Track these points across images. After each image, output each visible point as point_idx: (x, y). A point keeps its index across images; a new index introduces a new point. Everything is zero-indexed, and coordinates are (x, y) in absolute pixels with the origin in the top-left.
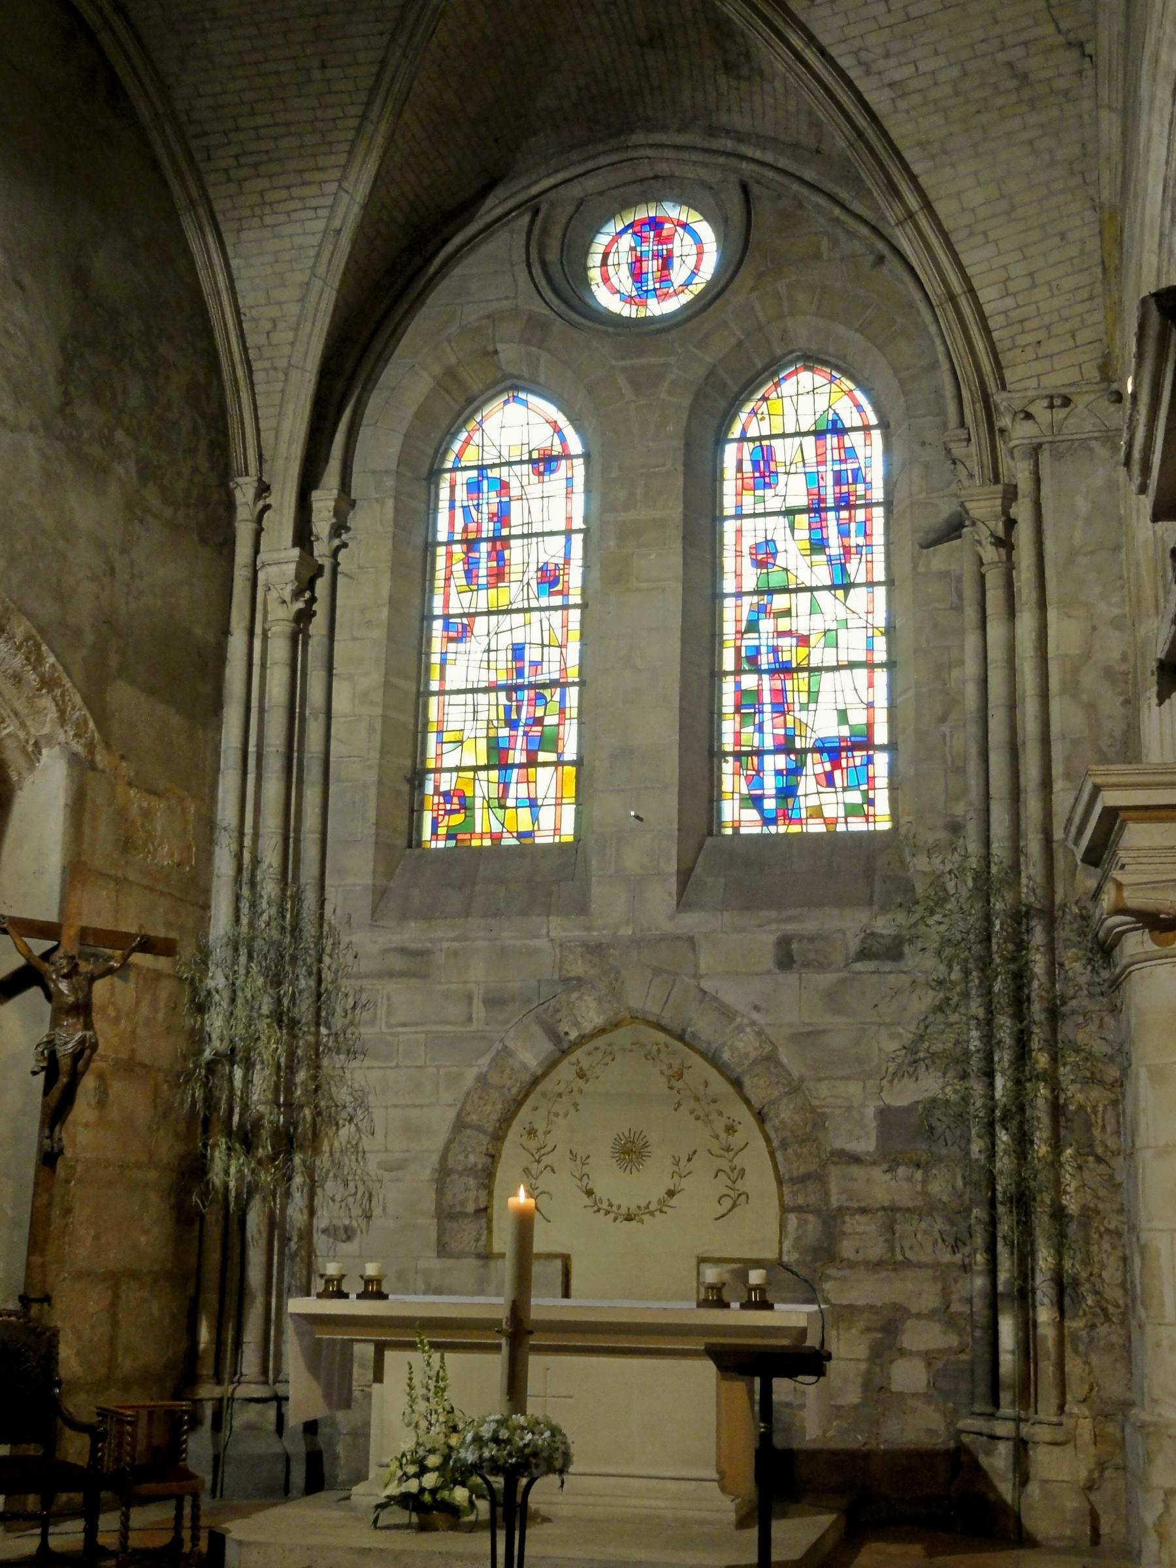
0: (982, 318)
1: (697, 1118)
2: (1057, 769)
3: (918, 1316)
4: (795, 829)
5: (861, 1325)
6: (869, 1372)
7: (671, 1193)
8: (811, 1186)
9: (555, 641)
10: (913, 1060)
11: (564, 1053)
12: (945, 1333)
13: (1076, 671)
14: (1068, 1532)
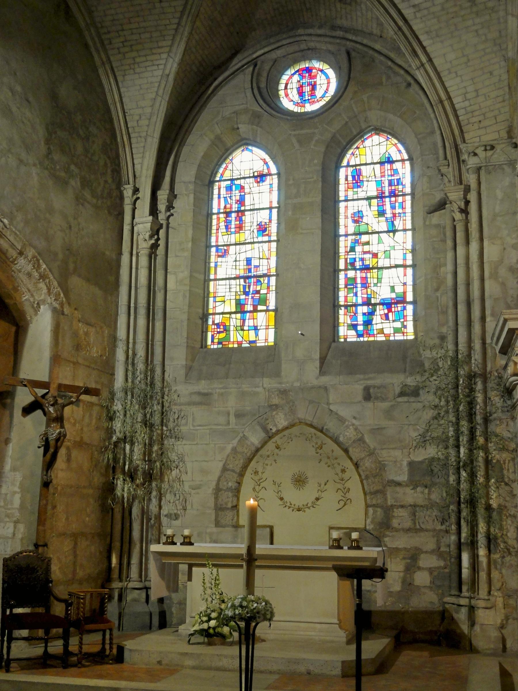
0: (455, 111)
1: (329, 466)
2: (488, 312)
3: (426, 552)
4: (371, 339)
7: (317, 499)
8: (379, 496)
9: (266, 257)
10: (424, 441)
11: (270, 438)
12: (438, 560)
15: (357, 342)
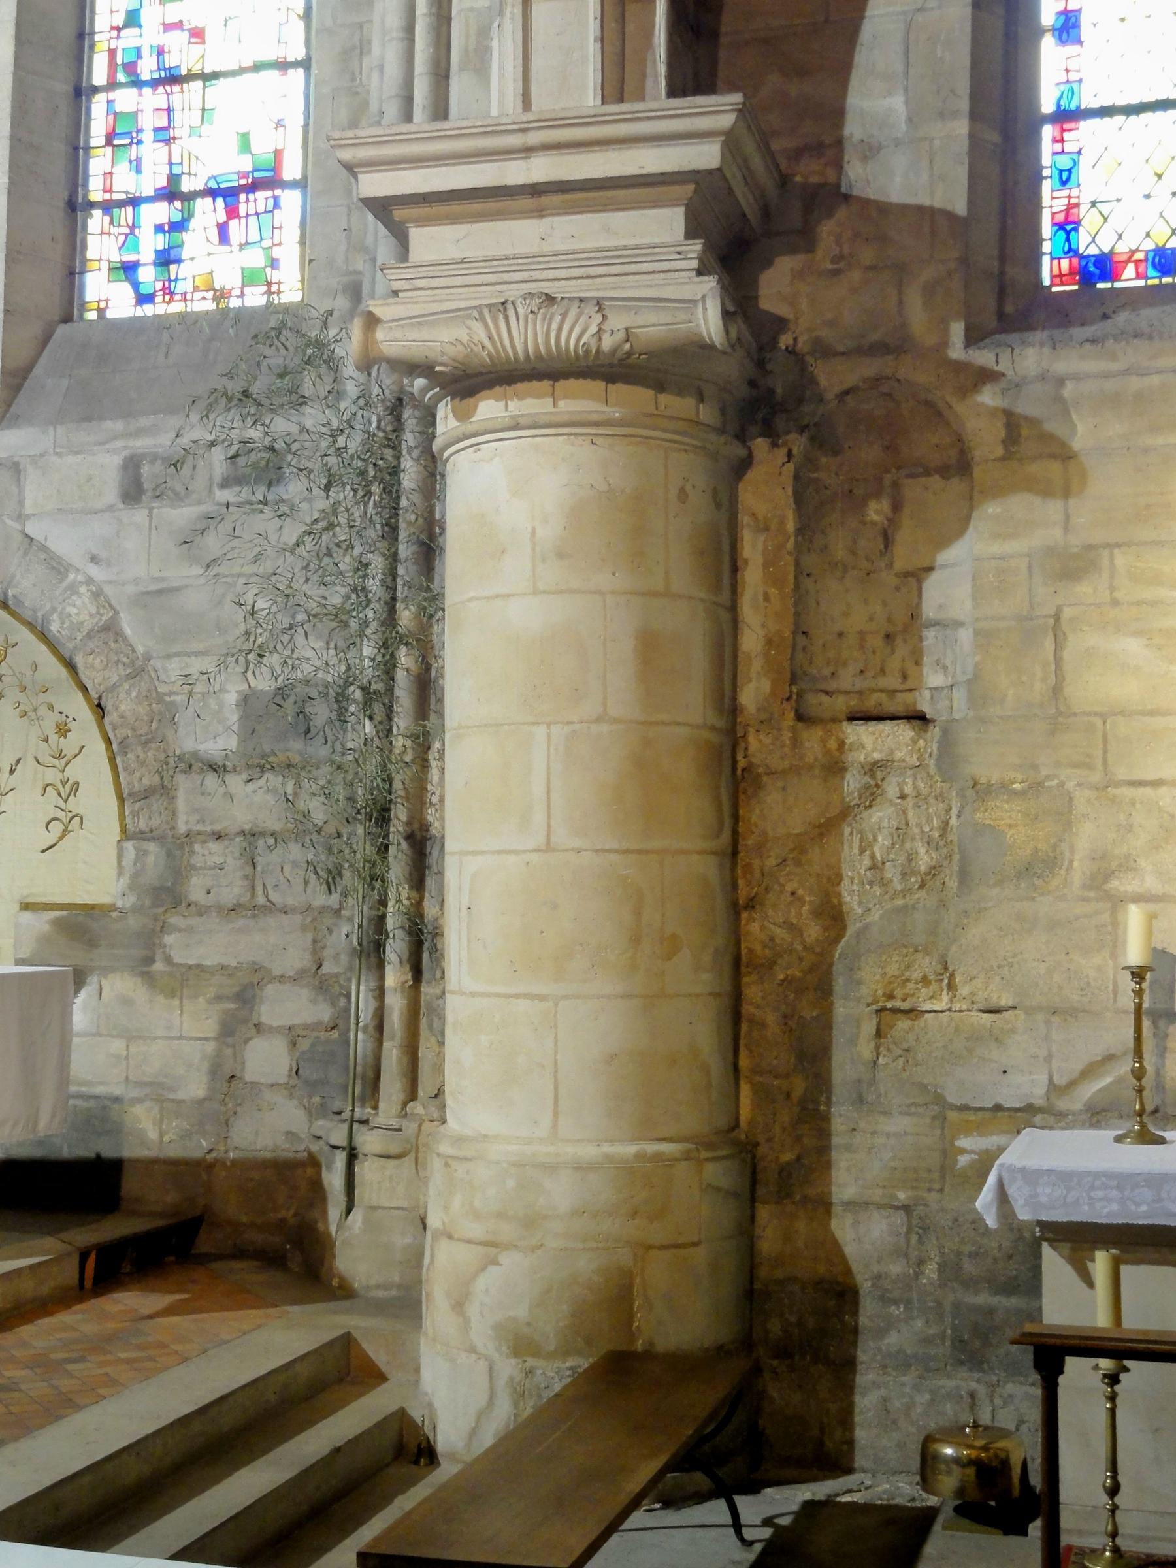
1: (24, 715)
3: (282, 979)
4: (176, 307)
5: (211, 992)
6: (218, 1055)
8: (157, 803)
12: (314, 1002)
14: (397, 1279)
15: (135, 319)
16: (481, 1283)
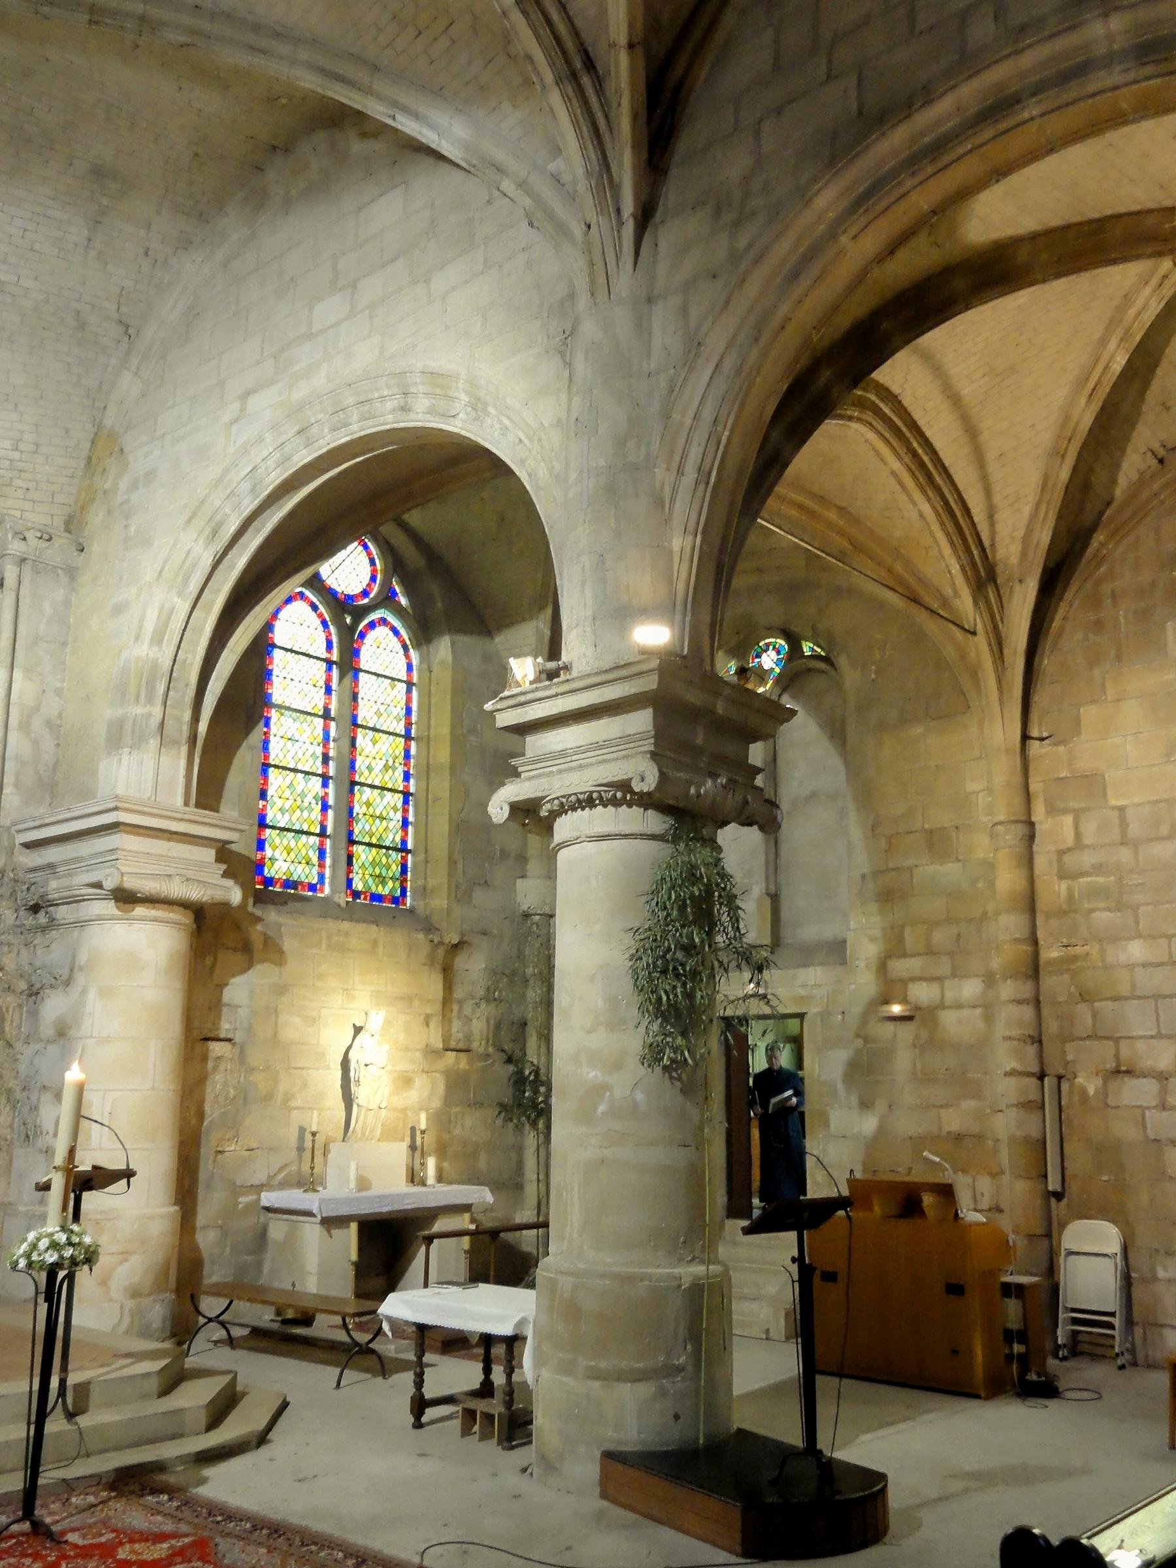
13: (30, 716)
16: (120, 1269)
